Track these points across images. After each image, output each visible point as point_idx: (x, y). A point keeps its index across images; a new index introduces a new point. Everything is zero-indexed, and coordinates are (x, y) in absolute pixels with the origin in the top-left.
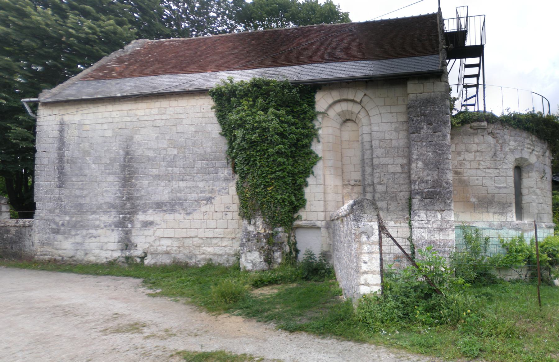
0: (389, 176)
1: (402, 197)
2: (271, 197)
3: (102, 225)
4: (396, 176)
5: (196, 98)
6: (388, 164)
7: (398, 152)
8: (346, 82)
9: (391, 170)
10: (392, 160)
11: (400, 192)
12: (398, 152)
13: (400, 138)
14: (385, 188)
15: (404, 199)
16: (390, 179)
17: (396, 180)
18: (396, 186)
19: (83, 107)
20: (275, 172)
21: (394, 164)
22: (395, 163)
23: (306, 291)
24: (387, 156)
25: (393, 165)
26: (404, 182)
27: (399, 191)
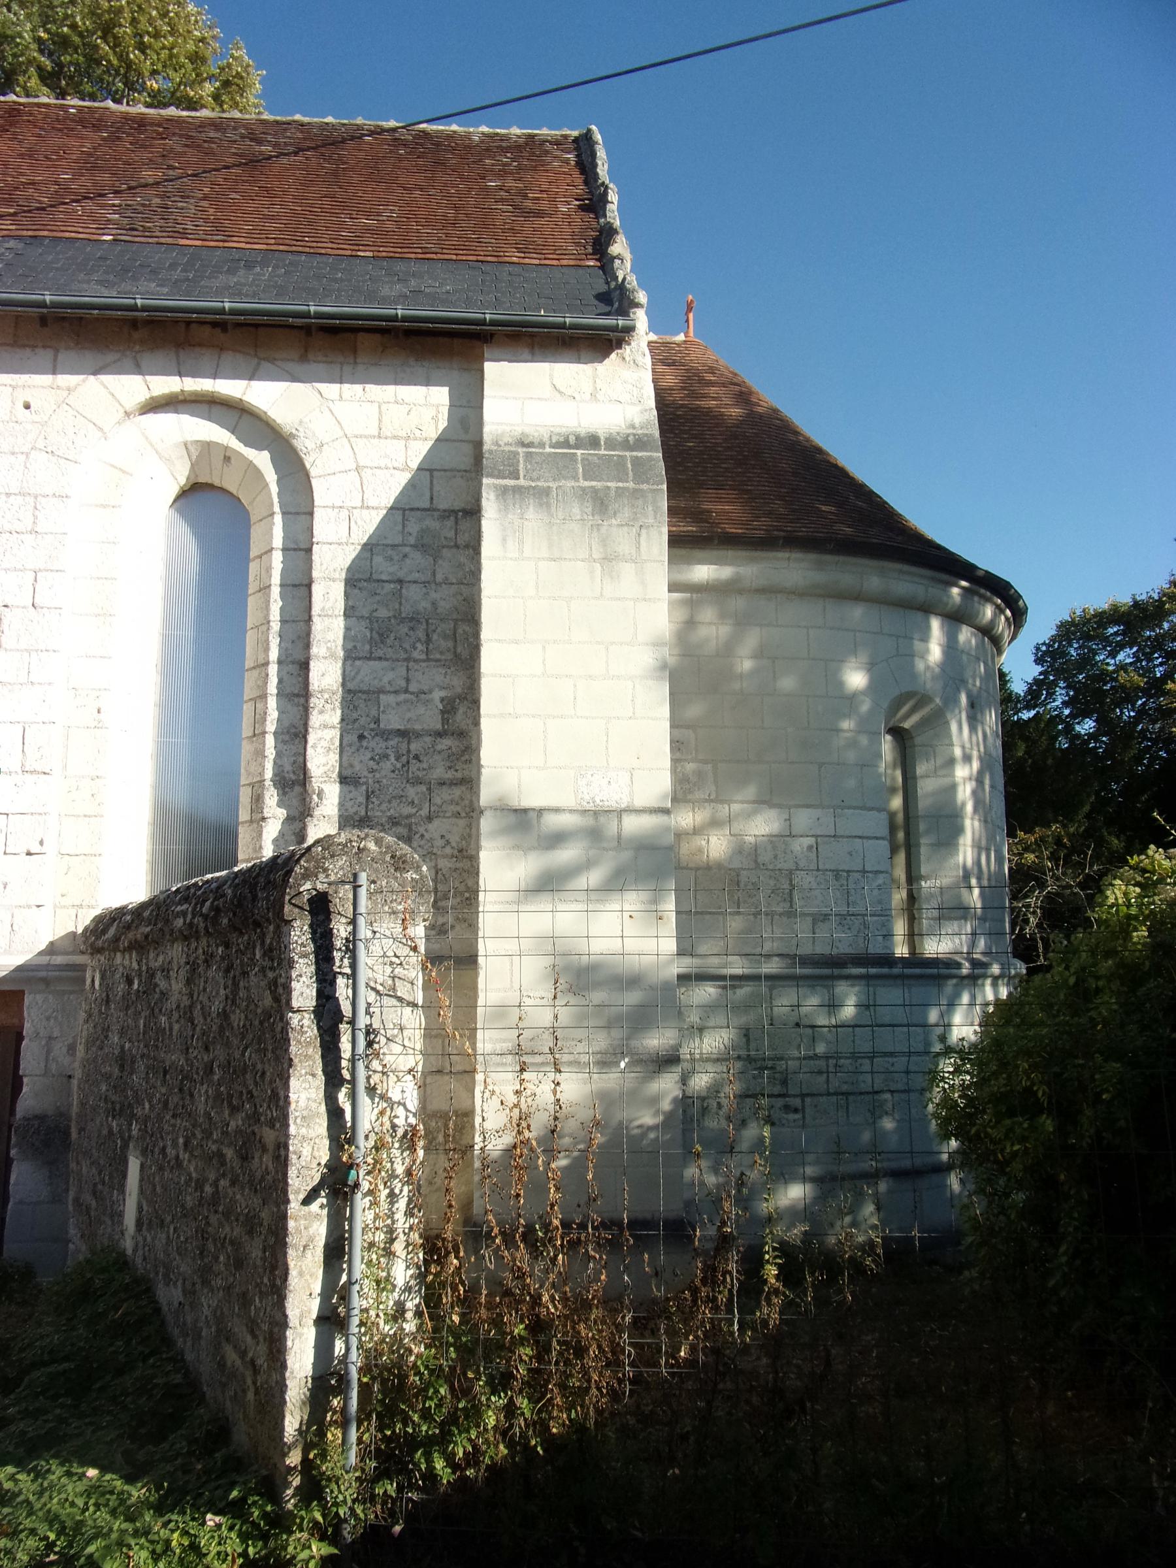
0: (378, 745)
1: (439, 842)
2: (1058, 879)
3: (558, 1097)
4: (415, 747)
5: (426, 364)
6: (382, 691)
7: (428, 640)
8: (124, 321)
9: (392, 721)
10: (403, 671)
11: (430, 819)
12: (428, 640)
13: (439, 577)
14: (362, 799)
15: (448, 850)
16: (386, 756)
17: (414, 766)
18: (412, 792)
19: (327, 356)
20: (697, 751)
21: (406, 691)
22: (413, 687)
23: (75, 1465)
24: (380, 653)
25: (402, 697)
26: (450, 775)
27: (424, 812)
